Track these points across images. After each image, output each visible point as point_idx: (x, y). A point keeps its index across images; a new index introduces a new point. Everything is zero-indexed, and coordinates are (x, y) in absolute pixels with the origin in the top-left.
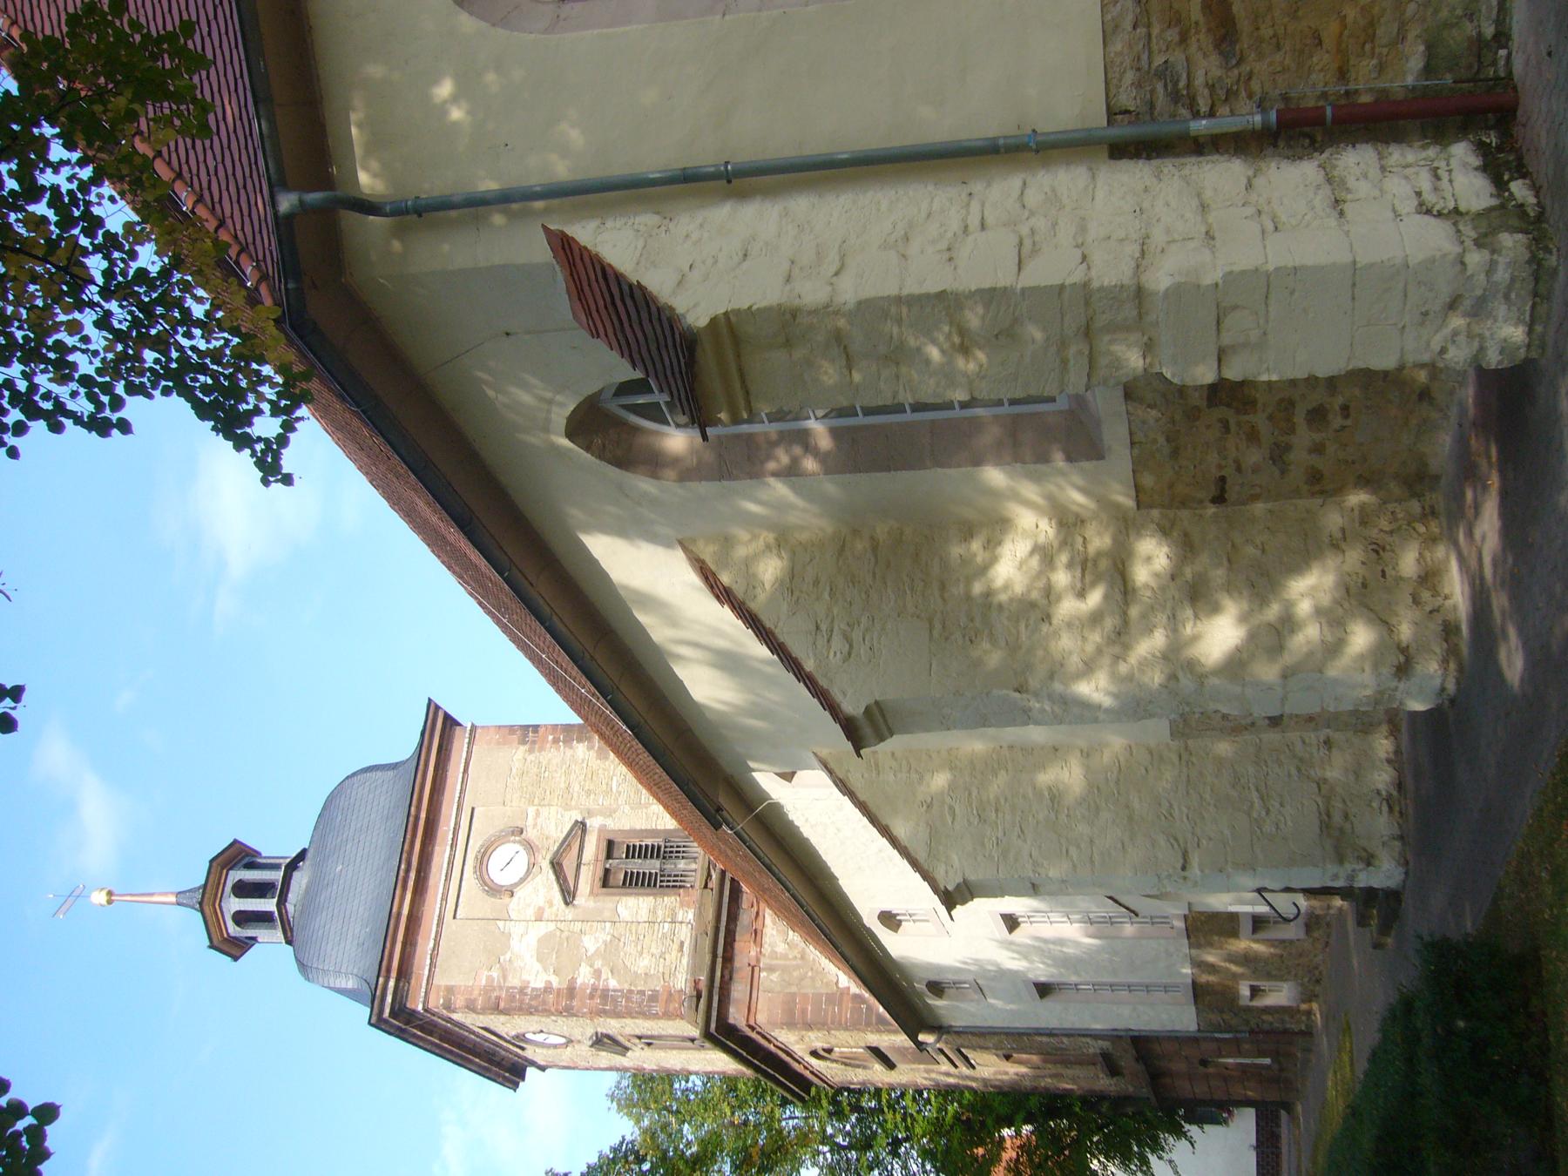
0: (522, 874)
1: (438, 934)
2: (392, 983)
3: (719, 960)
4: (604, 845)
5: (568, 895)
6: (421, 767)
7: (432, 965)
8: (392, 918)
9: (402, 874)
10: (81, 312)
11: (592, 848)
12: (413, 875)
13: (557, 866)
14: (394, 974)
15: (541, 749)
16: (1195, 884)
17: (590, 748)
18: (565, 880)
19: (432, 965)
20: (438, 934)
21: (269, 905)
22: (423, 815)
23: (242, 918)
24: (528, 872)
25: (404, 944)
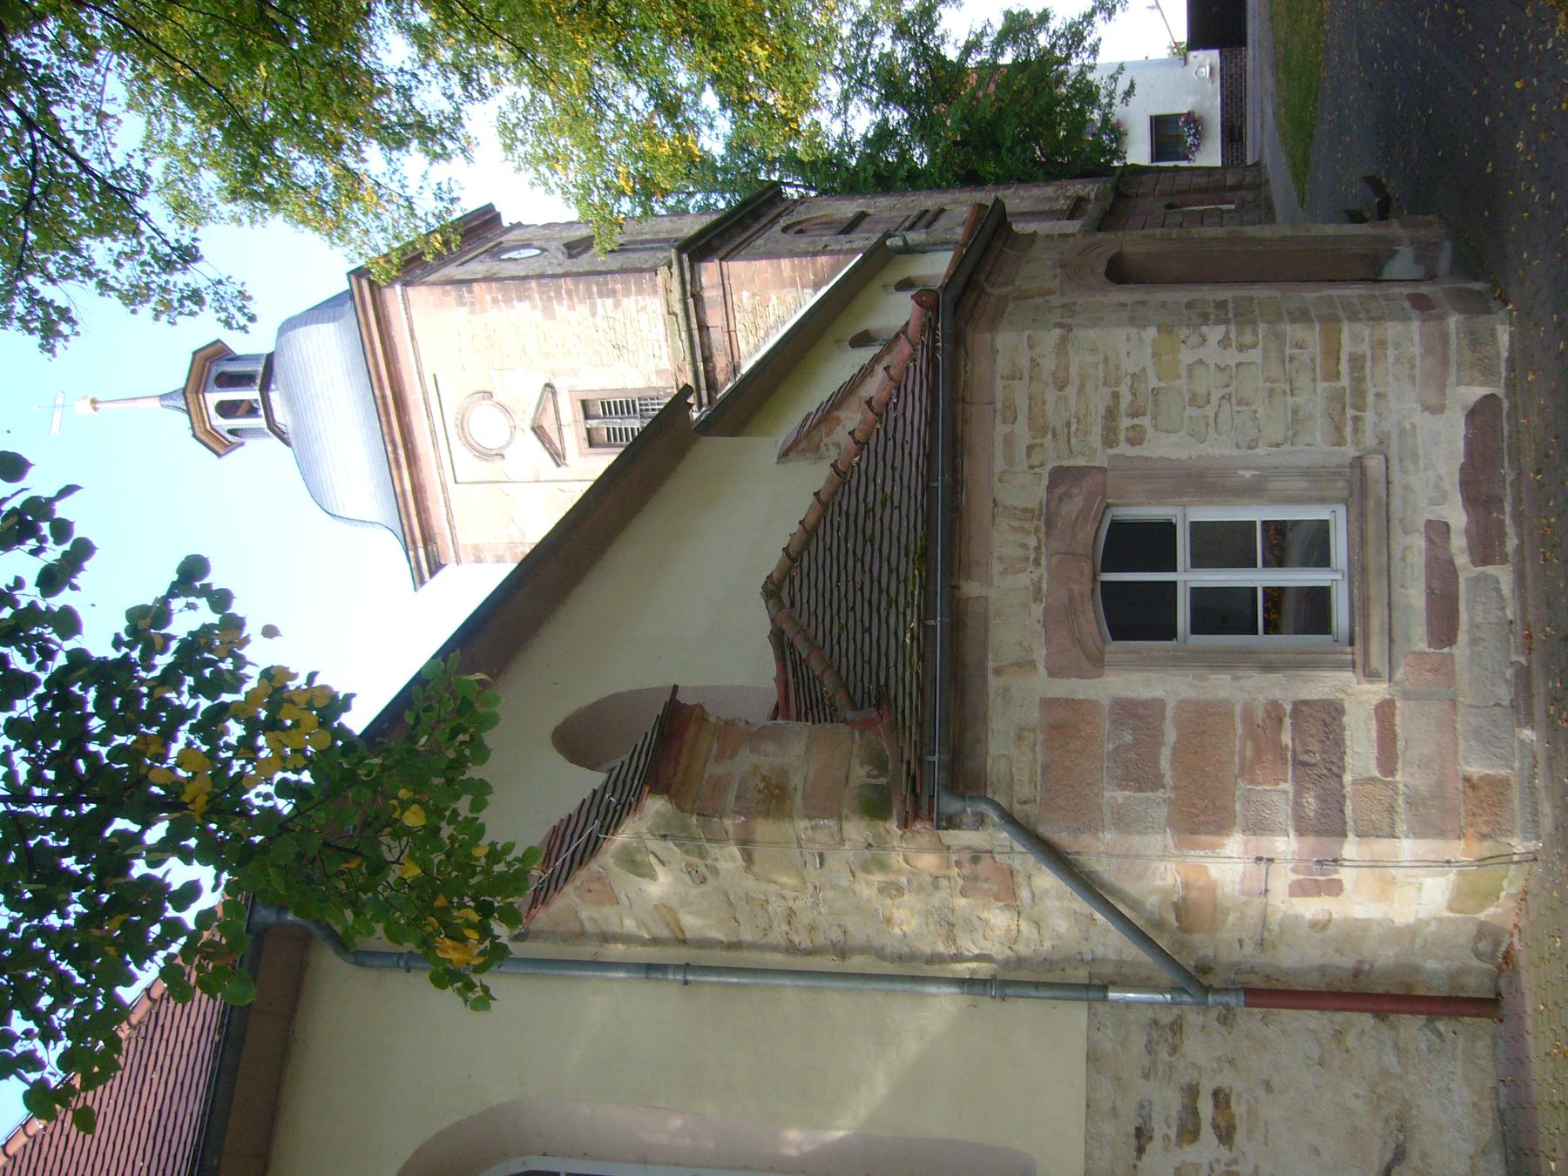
0: (507, 437)
1: (447, 500)
2: (421, 552)
3: (696, 333)
4: (579, 404)
5: (558, 457)
6: (368, 347)
7: (452, 528)
8: (399, 497)
9: (391, 456)
10: (33, 605)
11: (569, 411)
12: (401, 452)
13: (538, 431)
14: (420, 544)
15: (483, 310)
16: (1197, 146)
17: (534, 307)
18: (551, 443)
19: (452, 528)
20: (447, 500)
21: (251, 394)
22: (388, 393)
23: (226, 409)
24: (512, 435)
25: (419, 515)
